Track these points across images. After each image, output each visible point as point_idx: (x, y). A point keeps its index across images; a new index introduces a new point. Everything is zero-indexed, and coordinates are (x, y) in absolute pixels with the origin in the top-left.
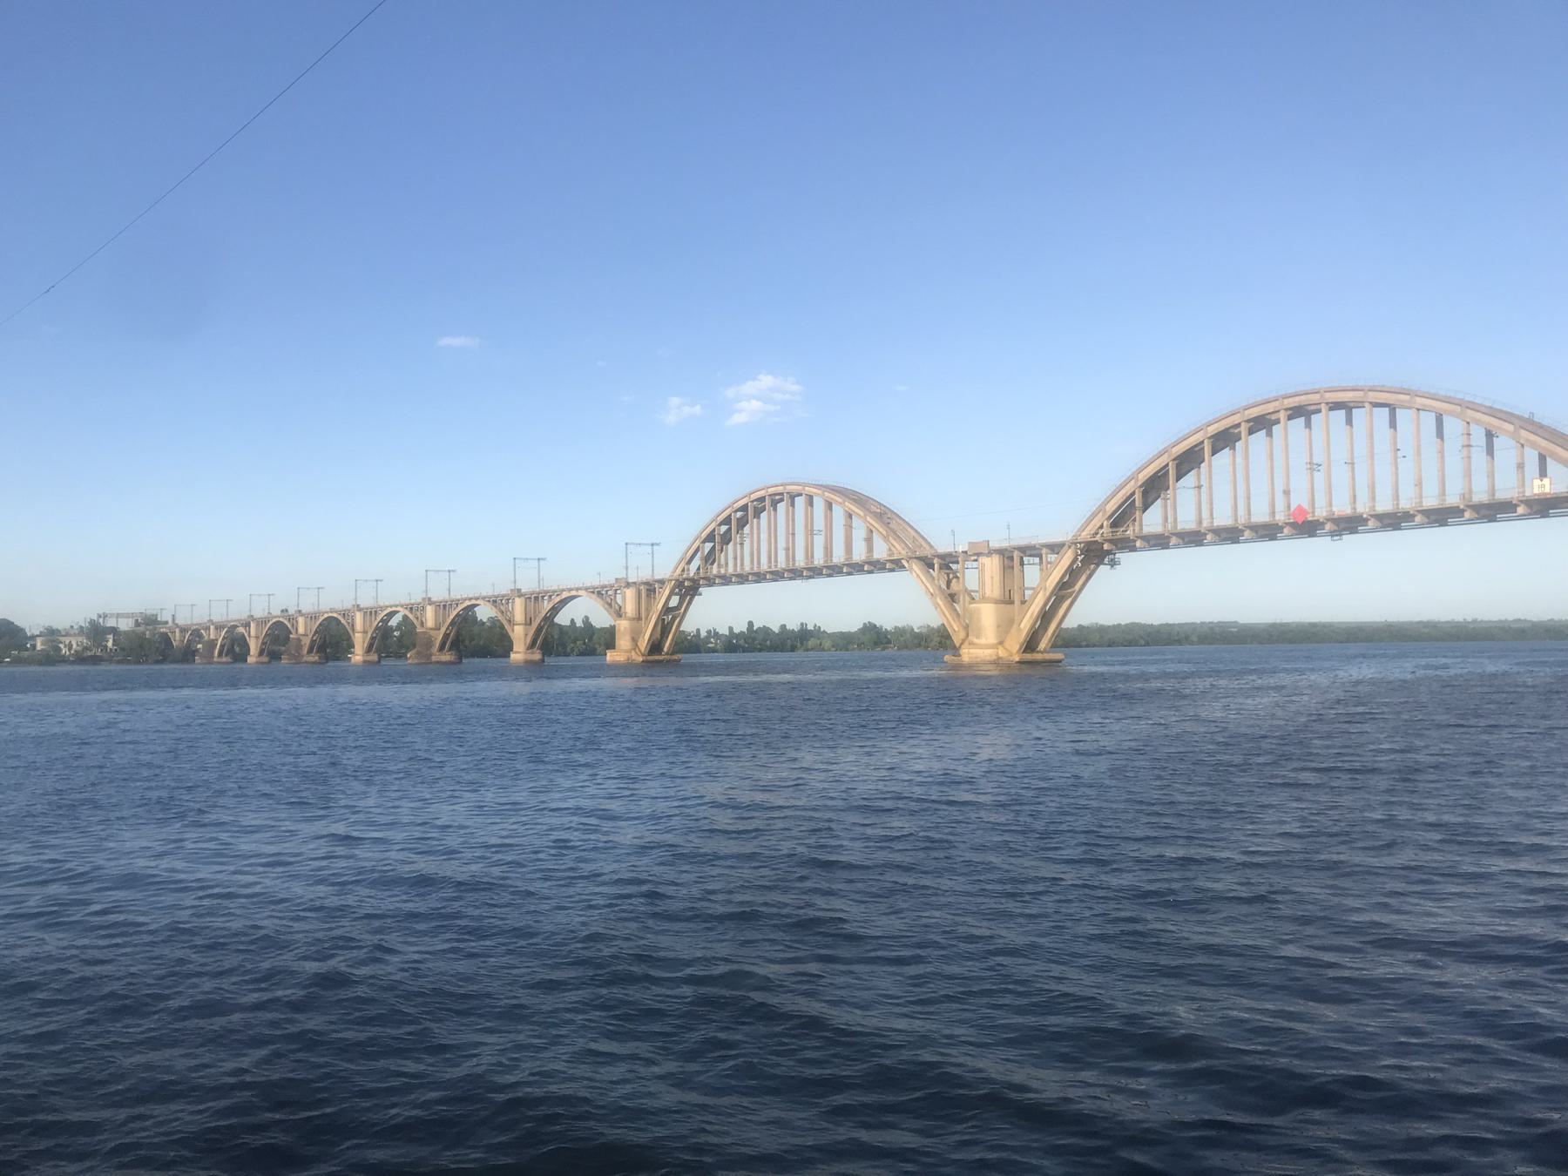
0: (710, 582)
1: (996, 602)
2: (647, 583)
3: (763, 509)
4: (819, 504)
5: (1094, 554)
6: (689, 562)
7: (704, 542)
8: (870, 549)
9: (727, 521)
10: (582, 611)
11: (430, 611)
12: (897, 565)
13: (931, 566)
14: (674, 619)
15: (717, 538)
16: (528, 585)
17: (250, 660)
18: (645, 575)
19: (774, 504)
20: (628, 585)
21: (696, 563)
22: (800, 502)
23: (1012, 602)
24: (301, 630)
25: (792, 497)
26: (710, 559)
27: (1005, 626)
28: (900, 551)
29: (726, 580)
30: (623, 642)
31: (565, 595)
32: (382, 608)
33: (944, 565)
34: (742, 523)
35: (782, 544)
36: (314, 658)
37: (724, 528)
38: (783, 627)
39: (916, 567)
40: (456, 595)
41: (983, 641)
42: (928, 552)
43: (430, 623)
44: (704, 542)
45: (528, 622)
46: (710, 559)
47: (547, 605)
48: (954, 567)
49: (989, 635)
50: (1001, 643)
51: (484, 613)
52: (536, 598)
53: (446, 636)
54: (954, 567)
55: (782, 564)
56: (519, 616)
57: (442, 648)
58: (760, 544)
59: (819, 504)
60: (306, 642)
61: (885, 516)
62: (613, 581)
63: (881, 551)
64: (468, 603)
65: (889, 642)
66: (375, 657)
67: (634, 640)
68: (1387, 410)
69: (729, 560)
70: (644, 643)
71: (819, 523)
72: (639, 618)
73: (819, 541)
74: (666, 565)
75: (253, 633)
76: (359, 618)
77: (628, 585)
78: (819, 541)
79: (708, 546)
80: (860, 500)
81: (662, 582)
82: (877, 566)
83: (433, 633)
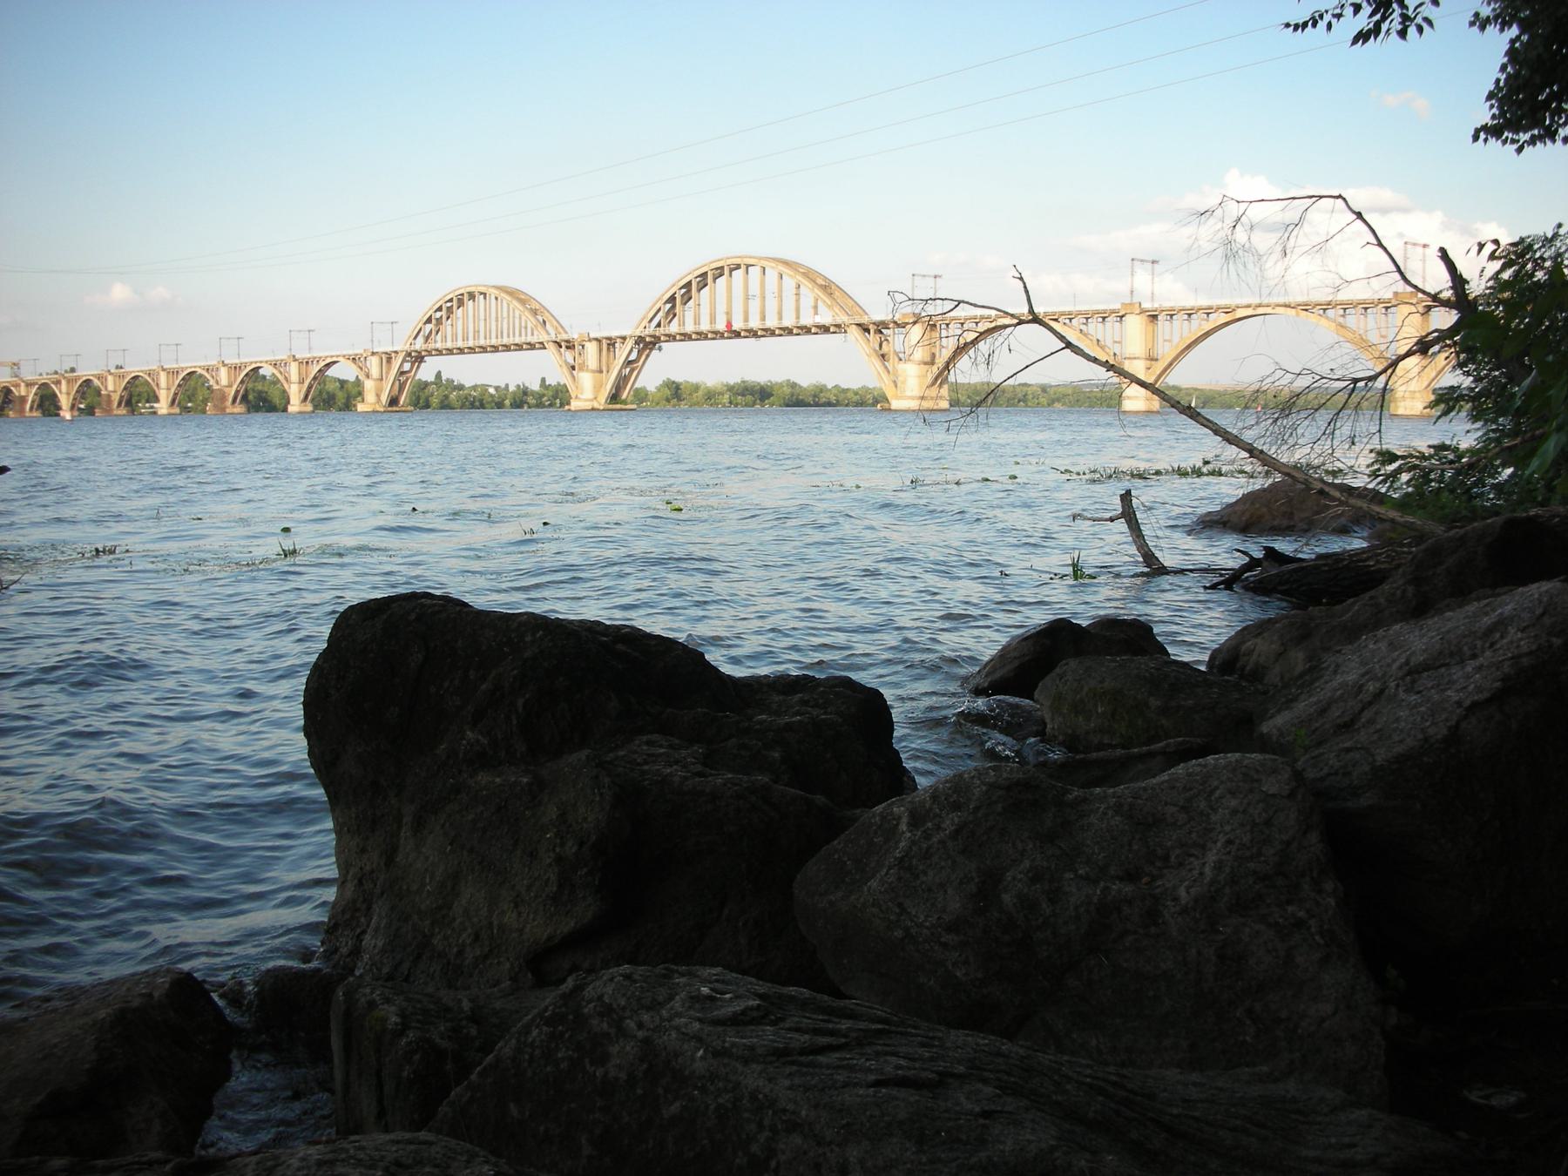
2: (609, 339)
5: (647, 344)
10: (345, 372)
13: (868, 331)
14: (632, 371)
16: (303, 355)
17: (291, 409)
18: (389, 349)
21: (420, 339)
22: (755, 272)
24: (111, 388)
27: (598, 387)
28: (842, 319)
29: (440, 352)
30: (370, 397)
39: (854, 332)
41: (908, 393)
42: (865, 320)
43: (224, 382)
45: (301, 382)
47: (315, 369)
49: (588, 393)
51: (267, 371)
53: (237, 392)
56: (294, 377)
57: (234, 401)
58: (702, 312)
59: (772, 275)
60: (116, 398)
61: (828, 288)
63: (825, 318)
65: (770, 395)
66: (309, 408)
67: (378, 396)
69: (688, 320)
70: (384, 398)
71: (754, 288)
73: (754, 306)
74: (629, 324)
76: (294, 369)
78: (754, 306)
80: (810, 275)
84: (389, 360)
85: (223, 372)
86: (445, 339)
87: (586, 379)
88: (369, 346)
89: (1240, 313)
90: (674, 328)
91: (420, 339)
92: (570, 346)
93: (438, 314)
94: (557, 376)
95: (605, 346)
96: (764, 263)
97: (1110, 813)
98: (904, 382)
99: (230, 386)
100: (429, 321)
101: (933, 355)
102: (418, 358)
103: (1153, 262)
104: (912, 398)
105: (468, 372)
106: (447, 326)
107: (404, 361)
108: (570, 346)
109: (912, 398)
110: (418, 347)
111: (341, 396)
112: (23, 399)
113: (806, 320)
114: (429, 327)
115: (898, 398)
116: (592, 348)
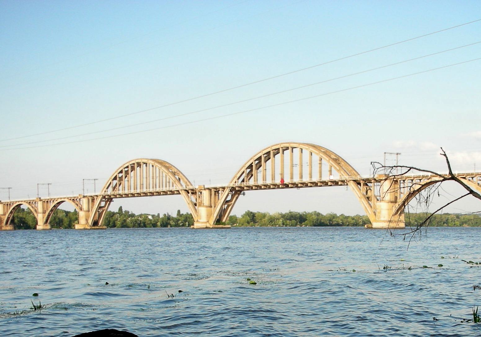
1: (207, 207)
2: (216, 188)
3: (278, 153)
4: (306, 153)
5: (237, 191)
7: (113, 180)
8: (292, 178)
15: (118, 179)
16: (45, 197)
20: (84, 197)
23: (211, 207)
27: (209, 215)
28: (345, 177)
29: (121, 196)
30: (82, 221)
31: (59, 201)
35: (148, 181)
36: (9, 227)
38: (246, 212)
39: (352, 185)
41: (382, 219)
42: (358, 178)
44: (113, 180)
45: (44, 212)
47: (52, 205)
48: (369, 184)
49: (204, 219)
50: (208, 221)
51: (25, 206)
52: (47, 202)
53: (8, 218)
54: (369, 184)
56: (40, 209)
58: (268, 173)
59: (306, 153)
61: (337, 160)
63: (336, 177)
64: (18, 203)
67: (87, 220)
68: (294, 149)
69: (259, 178)
70: (90, 221)
74: (227, 180)
76: (40, 205)
77: (84, 197)
78: (296, 170)
80: (327, 153)
83: (2, 217)
84: (93, 200)
87: (203, 211)
88: (81, 192)
90: (252, 182)
92: (194, 192)
94: (187, 209)
95: (213, 193)
96: (302, 146)
98: (380, 213)
99: (4, 215)
100: (115, 178)
101: (396, 198)
102: (109, 199)
104: (384, 221)
106: (125, 182)
107: (101, 201)
108: (194, 192)
109: (384, 221)
110: (109, 193)
111: (66, 220)
113: (325, 178)
115: (376, 221)
116: (206, 194)
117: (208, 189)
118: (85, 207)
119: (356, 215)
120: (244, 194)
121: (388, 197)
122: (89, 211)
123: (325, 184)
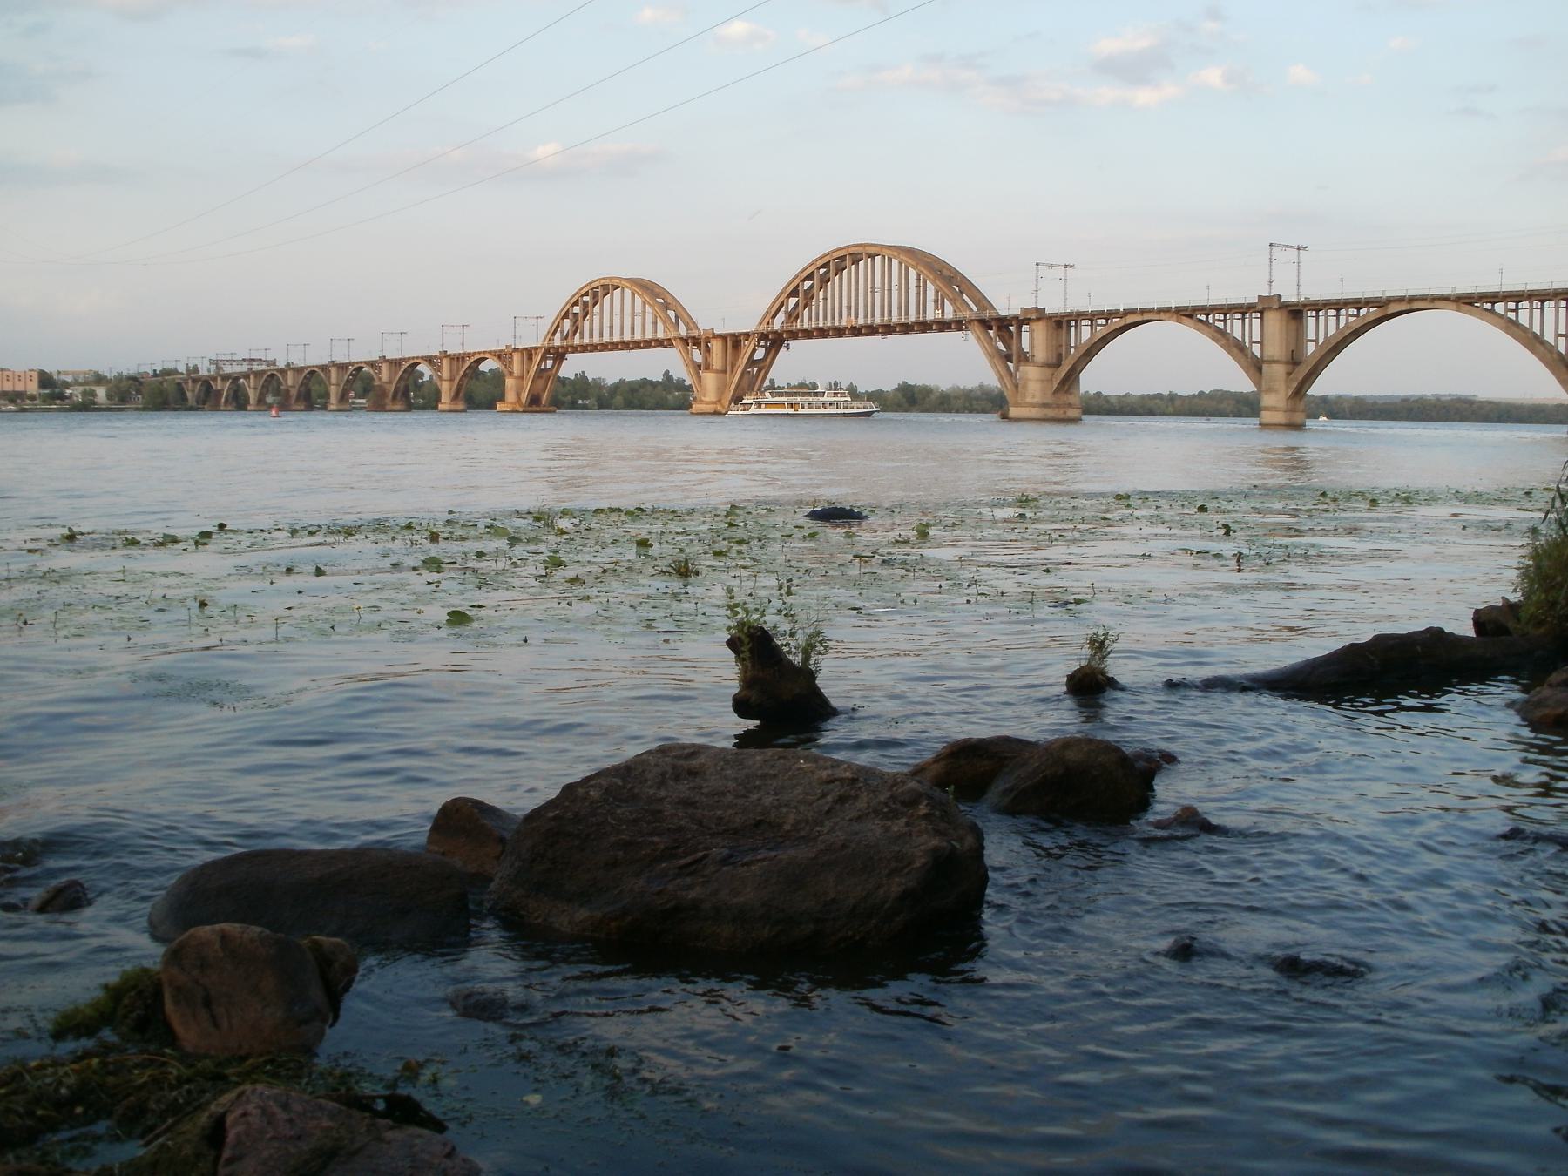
0: (794, 335)
1: (717, 372)
2: (733, 335)
5: (775, 342)
6: (774, 316)
7: (790, 295)
9: (810, 277)
11: (385, 368)
12: (958, 325)
15: (801, 294)
16: (1054, 306)
19: (856, 262)
20: (516, 350)
21: (781, 317)
22: (878, 259)
24: (290, 383)
25: (873, 257)
26: (793, 316)
27: (721, 389)
29: (808, 334)
32: (469, 355)
33: (1002, 327)
34: (825, 280)
37: (807, 284)
40: (469, 350)
41: (1029, 400)
43: (385, 377)
44: (790, 295)
45: (452, 380)
46: (793, 316)
49: (711, 396)
55: (912, 318)
56: (446, 373)
57: (394, 397)
59: (628, 292)
60: (294, 392)
62: (1017, 312)
67: (518, 395)
72: (725, 371)
75: (333, 380)
79: (792, 301)
81: (747, 335)
82: (943, 326)
84: (530, 358)
85: (385, 368)
86: (582, 337)
87: (710, 379)
88: (510, 342)
89: (1392, 309)
90: (577, 341)
91: (781, 317)
92: (696, 342)
93: (807, 284)
94: (681, 372)
95: (729, 344)
96: (887, 253)
97: (923, 809)
98: (1025, 387)
99: (390, 382)
100: (795, 293)
101: (1060, 356)
102: (559, 355)
103: (1299, 248)
104: (1033, 405)
105: (608, 369)
106: (818, 303)
107: (544, 358)
108: (696, 342)
109: (1033, 405)
110: (777, 327)
111: (225, 388)
112: (219, 393)
113: (932, 314)
114: (792, 301)
115: (1017, 405)
116: (716, 346)
117: (720, 336)
118: (516, 368)
119: (1166, 393)
120: (788, 347)
121: (1041, 354)
122: (725, 371)
123: (924, 327)
